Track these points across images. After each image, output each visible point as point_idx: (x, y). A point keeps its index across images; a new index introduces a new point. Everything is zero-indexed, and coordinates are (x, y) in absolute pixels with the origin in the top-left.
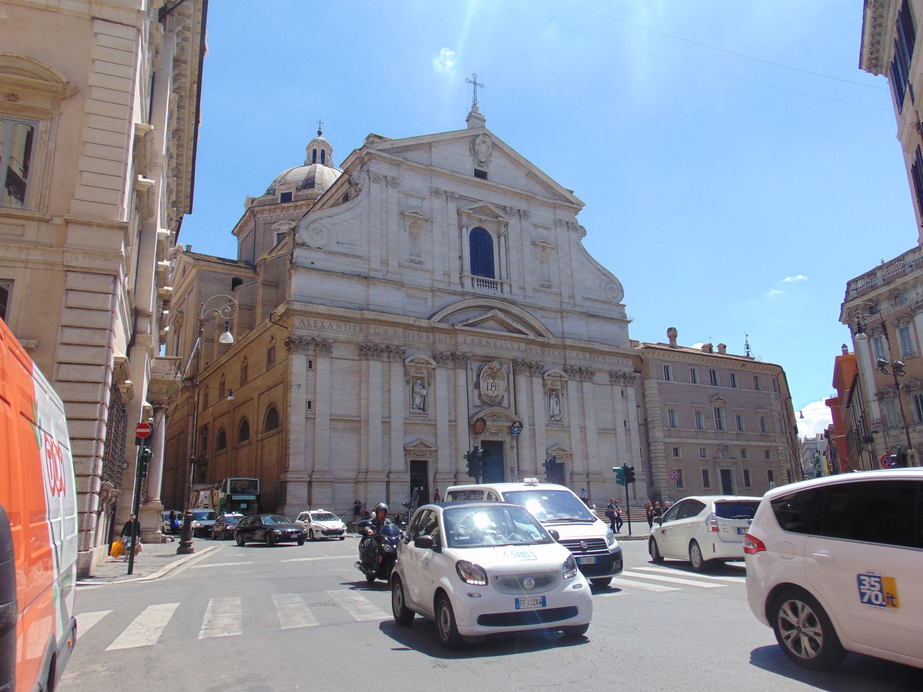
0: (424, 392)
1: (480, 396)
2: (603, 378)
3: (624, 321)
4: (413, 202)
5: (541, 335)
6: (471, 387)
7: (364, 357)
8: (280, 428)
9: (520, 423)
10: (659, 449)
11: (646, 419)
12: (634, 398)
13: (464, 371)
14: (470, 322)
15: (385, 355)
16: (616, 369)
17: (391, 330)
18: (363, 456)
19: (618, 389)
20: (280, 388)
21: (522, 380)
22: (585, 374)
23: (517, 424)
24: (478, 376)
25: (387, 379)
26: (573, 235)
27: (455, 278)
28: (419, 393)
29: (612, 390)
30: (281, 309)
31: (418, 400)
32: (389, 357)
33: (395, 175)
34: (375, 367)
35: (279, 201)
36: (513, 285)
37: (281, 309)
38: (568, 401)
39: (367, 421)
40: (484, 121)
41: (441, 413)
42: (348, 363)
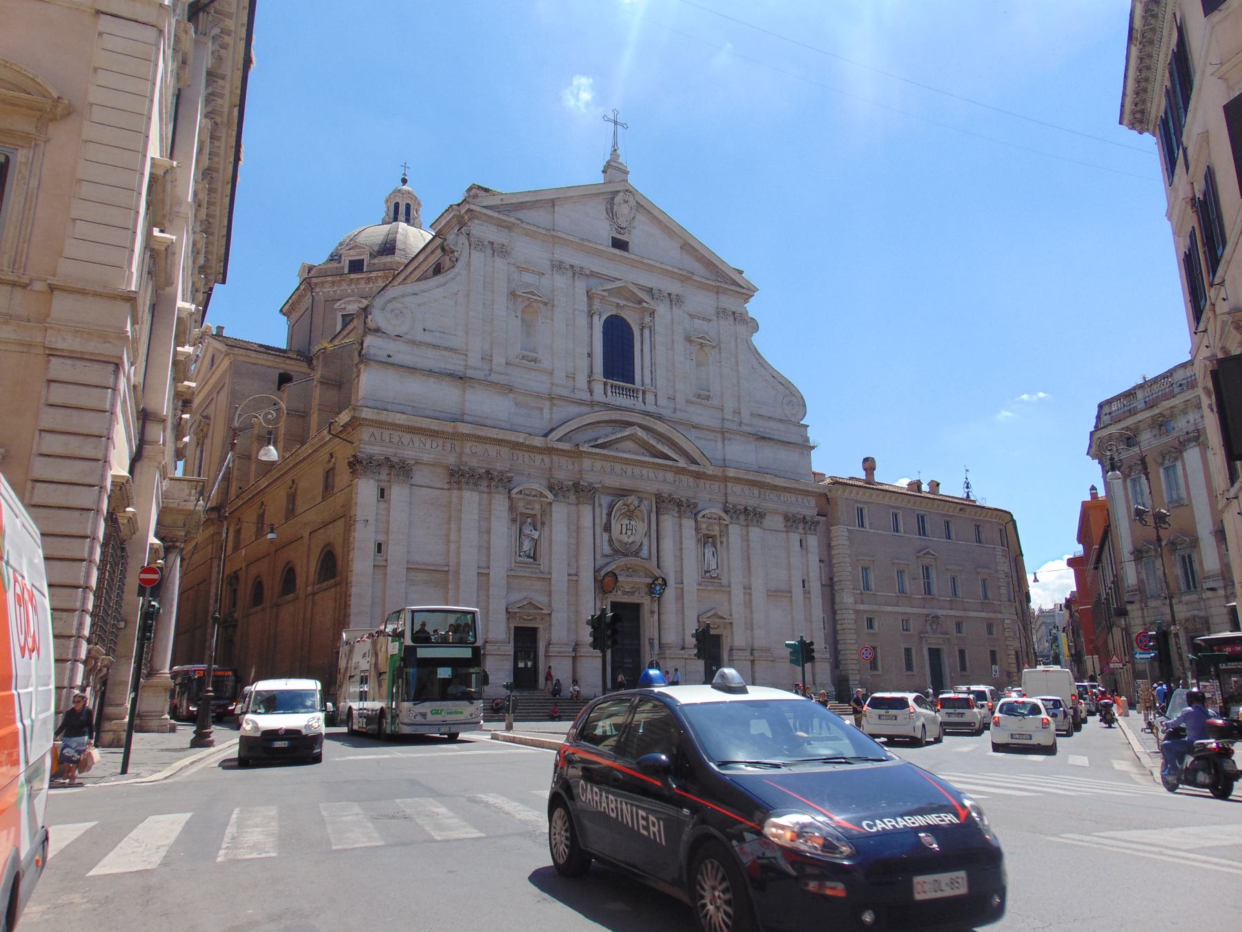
0: (536, 535)
1: (610, 541)
2: (776, 522)
3: (806, 447)
4: (528, 278)
5: (694, 462)
6: (598, 530)
7: (455, 486)
8: (338, 578)
9: (664, 580)
10: (847, 619)
11: (831, 579)
14: (600, 441)
19: (795, 538)
20: (341, 523)
21: (668, 522)
22: (752, 516)
23: (660, 581)
24: (609, 515)
25: (486, 516)
26: (741, 329)
27: (582, 381)
28: (528, 536)
30: (344, 417)
31: (527, 546)
33: (505, 242)
34: (471, 499)
35: (346, 271)
37: (344, 417)
39: (457, 572)
40: (627, 173)
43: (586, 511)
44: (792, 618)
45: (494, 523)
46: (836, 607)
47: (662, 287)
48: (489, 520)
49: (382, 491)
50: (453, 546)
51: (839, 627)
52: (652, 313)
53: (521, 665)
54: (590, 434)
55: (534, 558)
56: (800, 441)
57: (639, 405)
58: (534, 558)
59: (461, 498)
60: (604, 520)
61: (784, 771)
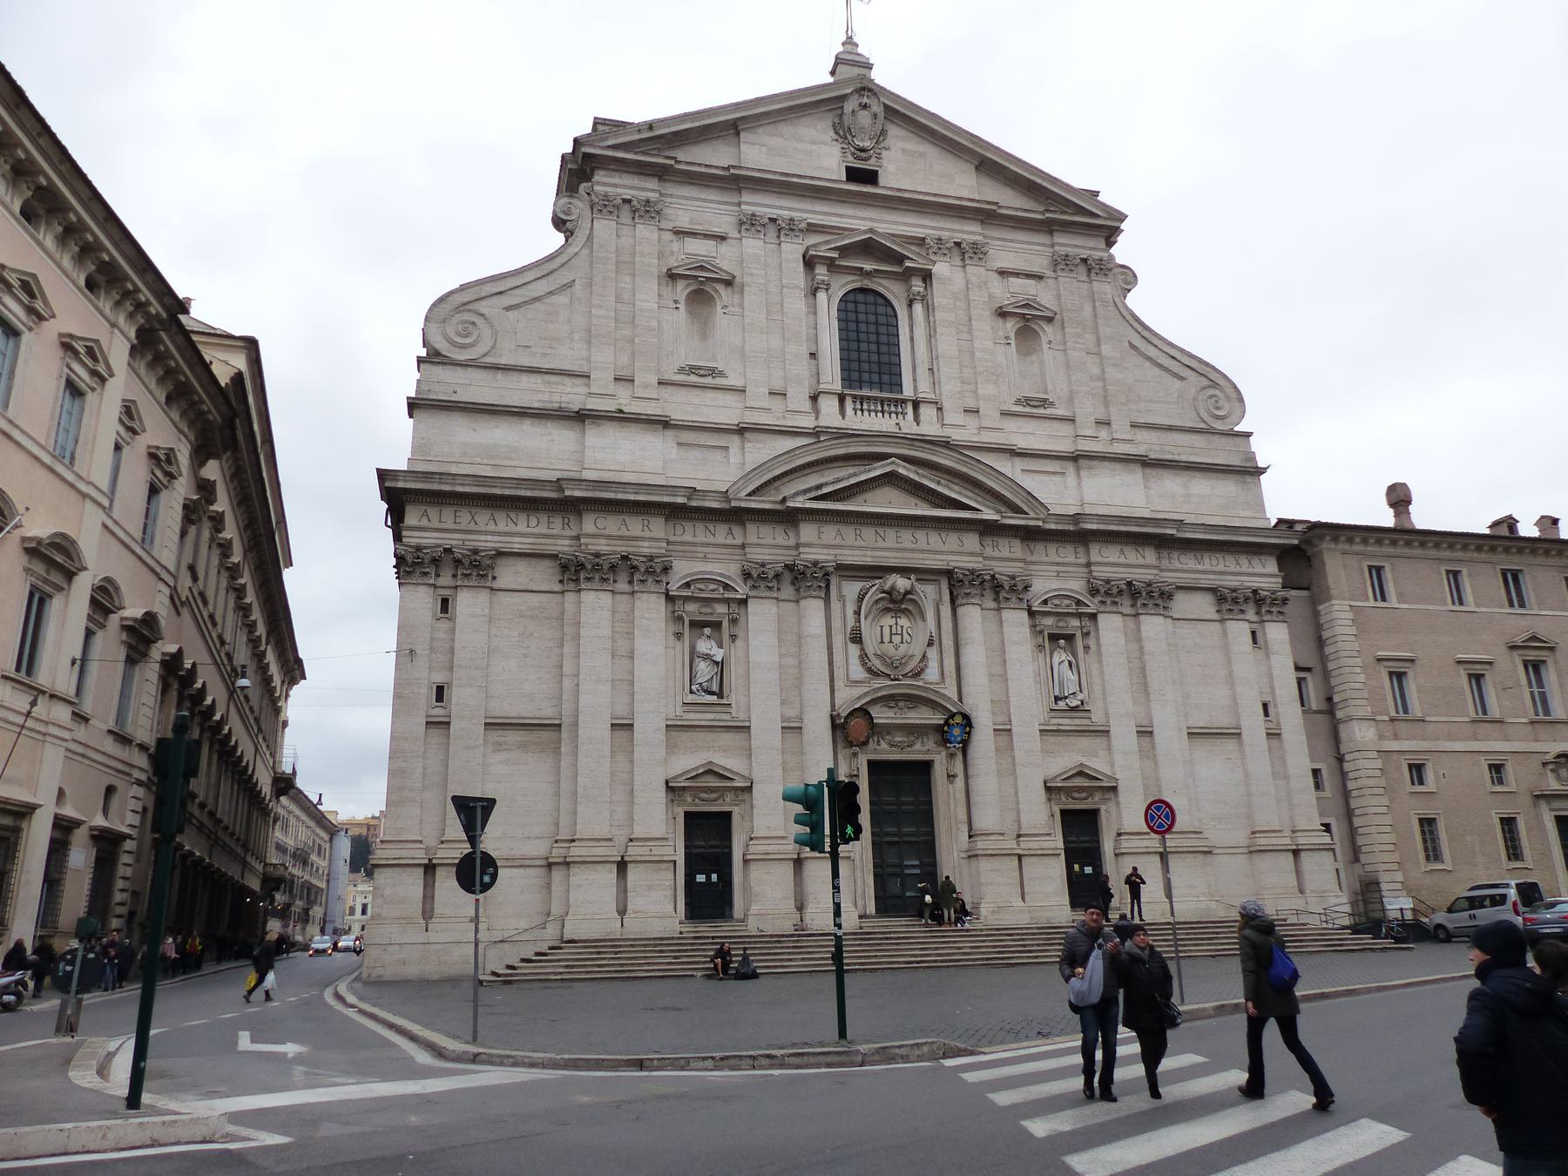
0: (718, 655)
1: (864, 657)
3: (1251, 472)
4: (697, 247)
5: (1017, 509)
6: (838, 640)
7: (572, 586)
9: (966, 717)
10: (1365, 768)
11: (1329, 699)
12: (1287, 648)
13: (820, 604)
14: (826, 490)
15: (623, 577)
16: (1231, 581)
17: (635, 525)
18: (565, 805)
19: (1239, 631)
22: (1146, 597)
23: (958, 719)
24: (858, 613)
25: (625, 630)
26: (1104, 288)
27: (799, 398)
28: (707, 657)
29: (1225, 634)
32: (630, 582)
33: (653, 196)
34: (596, 607)
36: (946, 406)
38: (1100, 661)
39: (576, 724)
40: (869, 67)
41: (760, 694)
42: (535, 600)
43: (813, 610)
44: (1247, 774)
45: (640, 643)
46: (1343, 749)
47: (945, 235)
48: (630, 635)
49: (445, 602)
50: (567, 683)
51: (1351, 785)
52: (927, 276)
53: (701, 878)
54: (812, 480)
55: (720, 695)
56: (1235, 460)
57: (908, 426)
58: (720, 695)
59: (579, 603)
60: (851, 622)
61: (351, 1013)
